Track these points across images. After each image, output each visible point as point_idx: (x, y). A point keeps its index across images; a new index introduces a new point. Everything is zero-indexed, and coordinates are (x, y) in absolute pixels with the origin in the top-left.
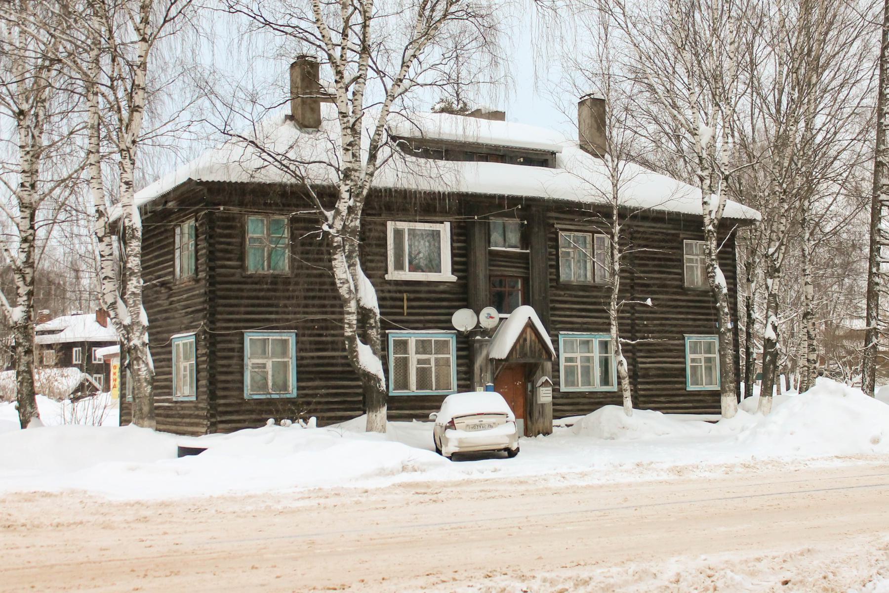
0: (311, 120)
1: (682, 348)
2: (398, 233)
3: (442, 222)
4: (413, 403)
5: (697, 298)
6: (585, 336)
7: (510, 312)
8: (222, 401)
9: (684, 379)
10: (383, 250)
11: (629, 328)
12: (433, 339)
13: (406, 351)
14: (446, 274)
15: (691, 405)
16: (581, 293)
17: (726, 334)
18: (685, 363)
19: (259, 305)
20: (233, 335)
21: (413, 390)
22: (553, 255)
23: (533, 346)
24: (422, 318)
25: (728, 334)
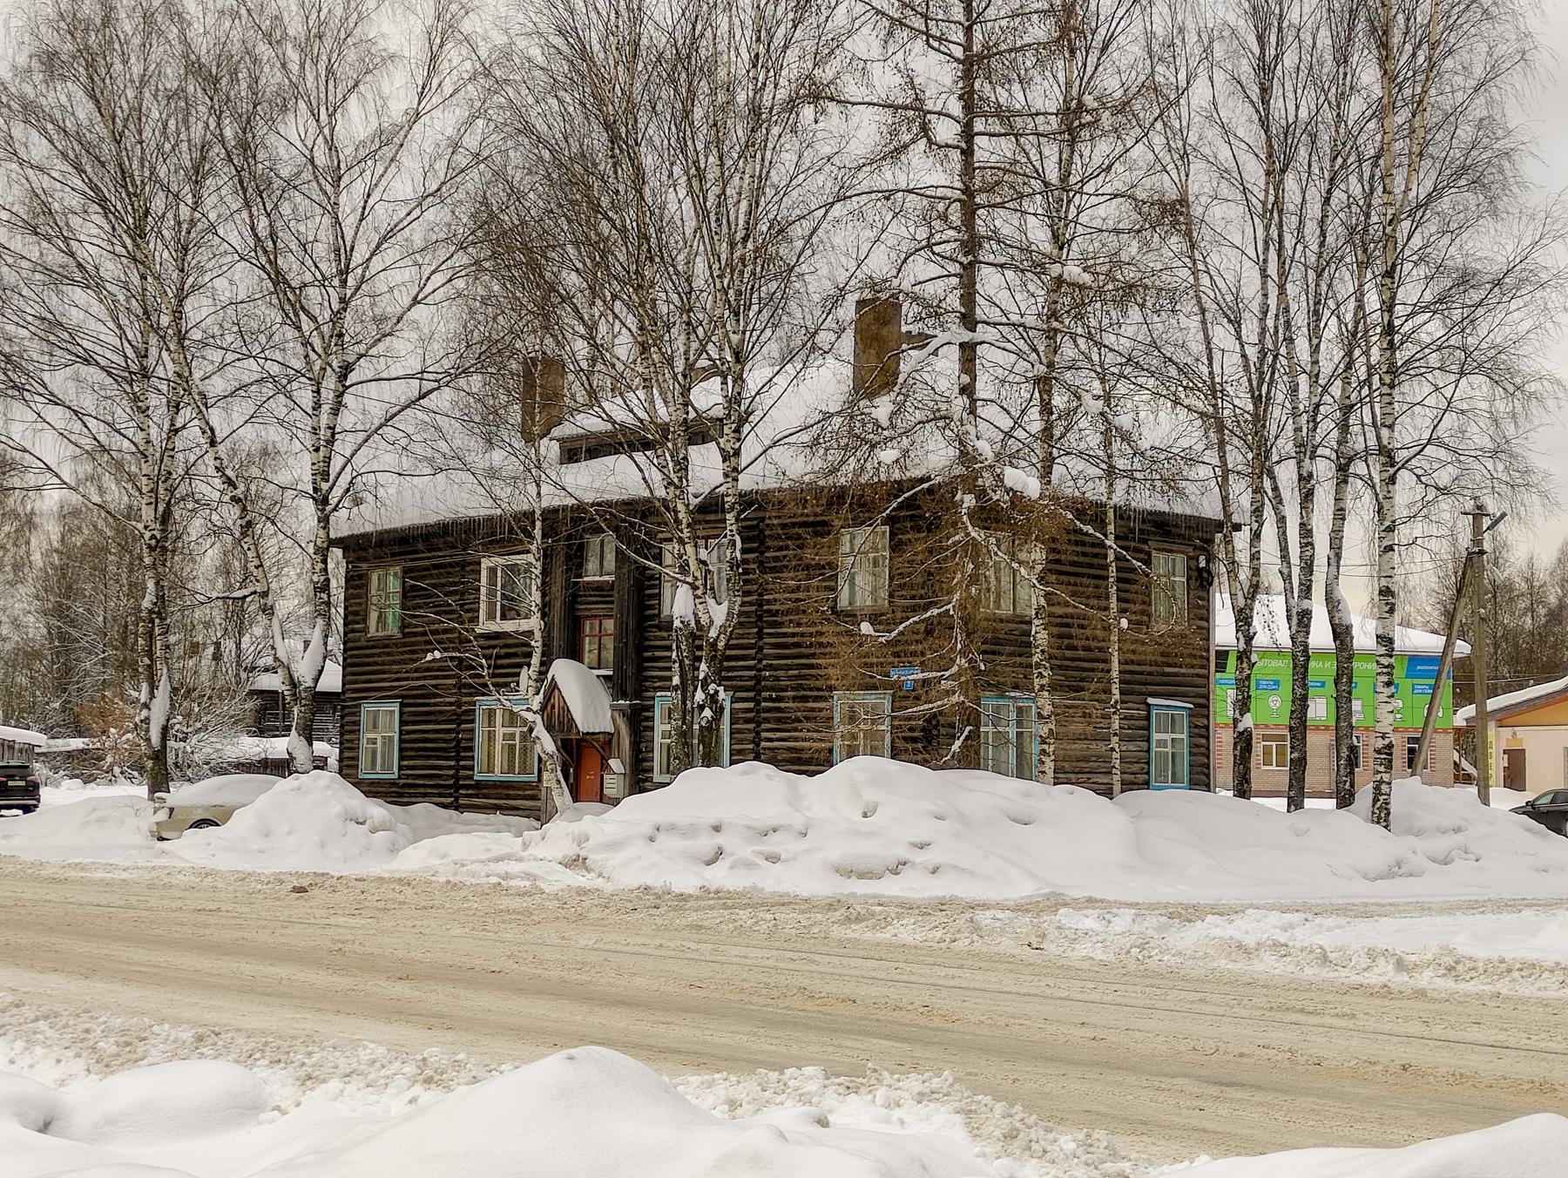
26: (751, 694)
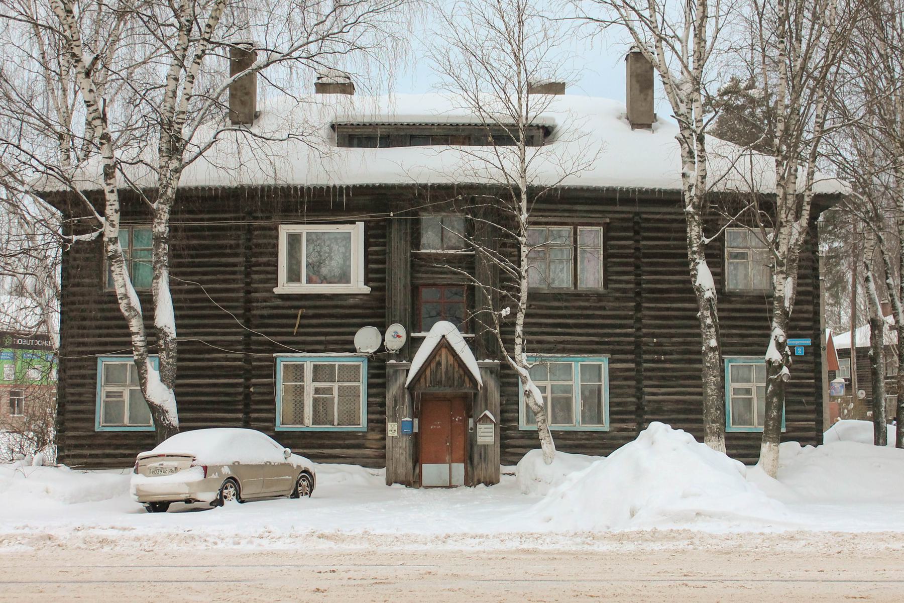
2: (294, 240)
3: (353, 222)
5: (744, 306)
6: (560, 359)
7: (428, 330)
10: (274, 259)
11: (632, 347)
12: (337, 364)
13: (302, 379)
14: (357, 285)
16: (556, 304)
17: (707, 354)
19: (204, 326)
20: (86, 360)
21: (309, 424)
22: (514, 256)
23: (450, 374)
24: (323, 338)
25: (711, 355)
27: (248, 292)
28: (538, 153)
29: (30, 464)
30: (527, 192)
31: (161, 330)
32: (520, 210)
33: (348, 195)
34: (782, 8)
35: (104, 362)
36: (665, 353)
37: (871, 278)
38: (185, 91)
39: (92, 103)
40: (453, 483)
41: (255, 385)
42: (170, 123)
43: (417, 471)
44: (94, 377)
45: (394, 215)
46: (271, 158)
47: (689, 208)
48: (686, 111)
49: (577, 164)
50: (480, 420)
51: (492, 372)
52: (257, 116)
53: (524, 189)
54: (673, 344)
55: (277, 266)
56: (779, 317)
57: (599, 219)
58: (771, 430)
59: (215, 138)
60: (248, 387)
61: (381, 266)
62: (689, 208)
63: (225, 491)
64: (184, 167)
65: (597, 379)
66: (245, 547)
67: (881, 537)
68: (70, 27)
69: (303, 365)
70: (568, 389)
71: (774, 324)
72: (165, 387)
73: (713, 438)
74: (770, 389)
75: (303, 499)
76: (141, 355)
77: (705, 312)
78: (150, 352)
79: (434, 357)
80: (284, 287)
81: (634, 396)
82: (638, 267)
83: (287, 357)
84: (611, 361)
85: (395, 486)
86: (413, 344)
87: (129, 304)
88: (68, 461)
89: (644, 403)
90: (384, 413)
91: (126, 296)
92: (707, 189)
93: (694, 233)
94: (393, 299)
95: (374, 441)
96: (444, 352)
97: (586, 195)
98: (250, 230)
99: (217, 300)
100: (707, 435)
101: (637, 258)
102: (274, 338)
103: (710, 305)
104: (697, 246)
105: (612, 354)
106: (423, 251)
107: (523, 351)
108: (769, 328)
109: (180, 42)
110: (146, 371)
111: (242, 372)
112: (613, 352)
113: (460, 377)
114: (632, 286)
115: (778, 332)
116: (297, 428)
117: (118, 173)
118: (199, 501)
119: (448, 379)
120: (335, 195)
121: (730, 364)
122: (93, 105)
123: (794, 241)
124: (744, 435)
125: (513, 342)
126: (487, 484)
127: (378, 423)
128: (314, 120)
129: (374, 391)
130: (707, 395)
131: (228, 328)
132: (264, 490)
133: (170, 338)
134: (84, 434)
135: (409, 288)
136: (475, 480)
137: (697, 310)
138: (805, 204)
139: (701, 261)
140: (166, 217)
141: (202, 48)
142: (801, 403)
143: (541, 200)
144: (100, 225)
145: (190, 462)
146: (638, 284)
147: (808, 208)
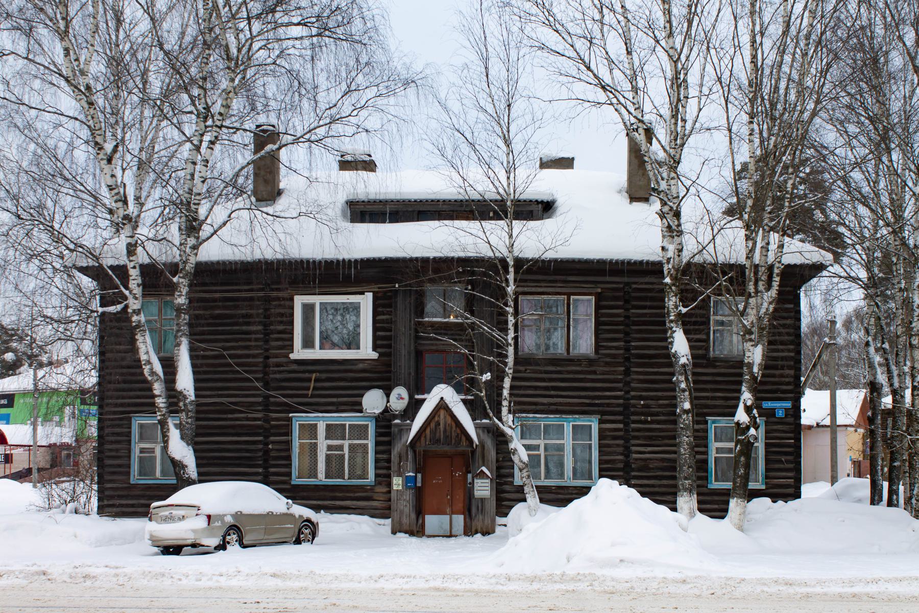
0: (264, 193)
1: (704, 434)
3: (362, 293)
4: (322, 493)
6: (552, 420)
7: (429, 392)
8: (109, 485)
9: (705, 474)
11: (621, 409)
12: (348, 423)
14: (366, 351)
15: (716, 506)
18: (706, 453)
24: (334, 400)
25: (684, 417)
26: (621, 418)
27: (267, 358)
28: (525, 229)
29: (64, 512)
30: (514, 266)
31: (181, 393)
32: (507, 280)
33: (356, 268)
34: (751, 90)
35: (138, 421)
36: (652, 415)
37: (871, 343)
38: (201, 175)
39: (114, 187)
40: (453, 533)
41: (273, 443)
42: (189, 203)
43: (420, 521)
44: (129, 434)
45: (399, 286)
46: (282, 236)
47: (668, 280)
48: (666, 187)
49: (554, 241)
50: (476, 476)
51: (488, 432)
52: (280, 193)
53: (511, 263)
54: (660, 406)
55: (293, 334)
56: (748, 382)
57: (591, 289)
58: (738, 487)
59: (229, 216)
60: (267, 444)
61: (388, 334)
62: (668, 280)
63: (228, 538)
64: (201, 244)
65: (588, 438)
66: (204, 583)
67: (761, 582)
68: (93, 118)
69: (316, 425)
70: (560, 448)
71: (744, 389)
72: (184, 444)
73: (685, 493)
74: (738, 448)
75: (305, 546)
76: (164, 415)
77: (680, 377)
78: (171, 412)
79: (434, 417)
80: (299, 353)
81: (621, 454)
82: (627, 334)
83: (302, 417)
84: (601, 422)
85: (399, 535)
86: (415, 406)
87: (151, 369)
88: (107, 509)
89: (631, 461)
90: (389, 468)
91: (149, 362)
92: (685, 261)
93: (671, 303)
94: (398, 364)
95: (381, 495)
96: (442, 413)
97: (578, 266)
98: (268, 300)
99: (238, 365)
100: (680, 491)
101: (627, 325)
102: (290, 399)
103: (685, 370)
104: (675, 315)
105: (602, 416)
106: (427, 319)
107: (510, 412)
108: (739, 391)
109: (198, 128)
110: (168, 429)
111: (261, 431)
112: (602, 413)
113: (457, 436)
114: (621, 352)
115: (747, 396)
116: (311, 481)
117: (140, 249)
118: (203, 546)
119: (446, 437)
120: (344, 268)
121: (713, 425)
122: (114, 189)
123: (765, 310)
124: (725, 491)
125: (500, 404)
126: (484, 534)
127: (384, 478)
128: (324, 197)
129: (381, 448)
130: (680, 454)
131: (249, 390)
132: (266, 537)
133: (189, 400)
134: (121, 486)
135: (413, 355)
136: (473, 530)
137: (673, 374)
138: (775, 275)
139: (678, 329)
140: (185, 290)
141: (215, 134)
142: (780, 462)
143: (529, 271)
144: (126, 298)
145: (195, 511)
146: (627, 349)
147: (778, 279)
